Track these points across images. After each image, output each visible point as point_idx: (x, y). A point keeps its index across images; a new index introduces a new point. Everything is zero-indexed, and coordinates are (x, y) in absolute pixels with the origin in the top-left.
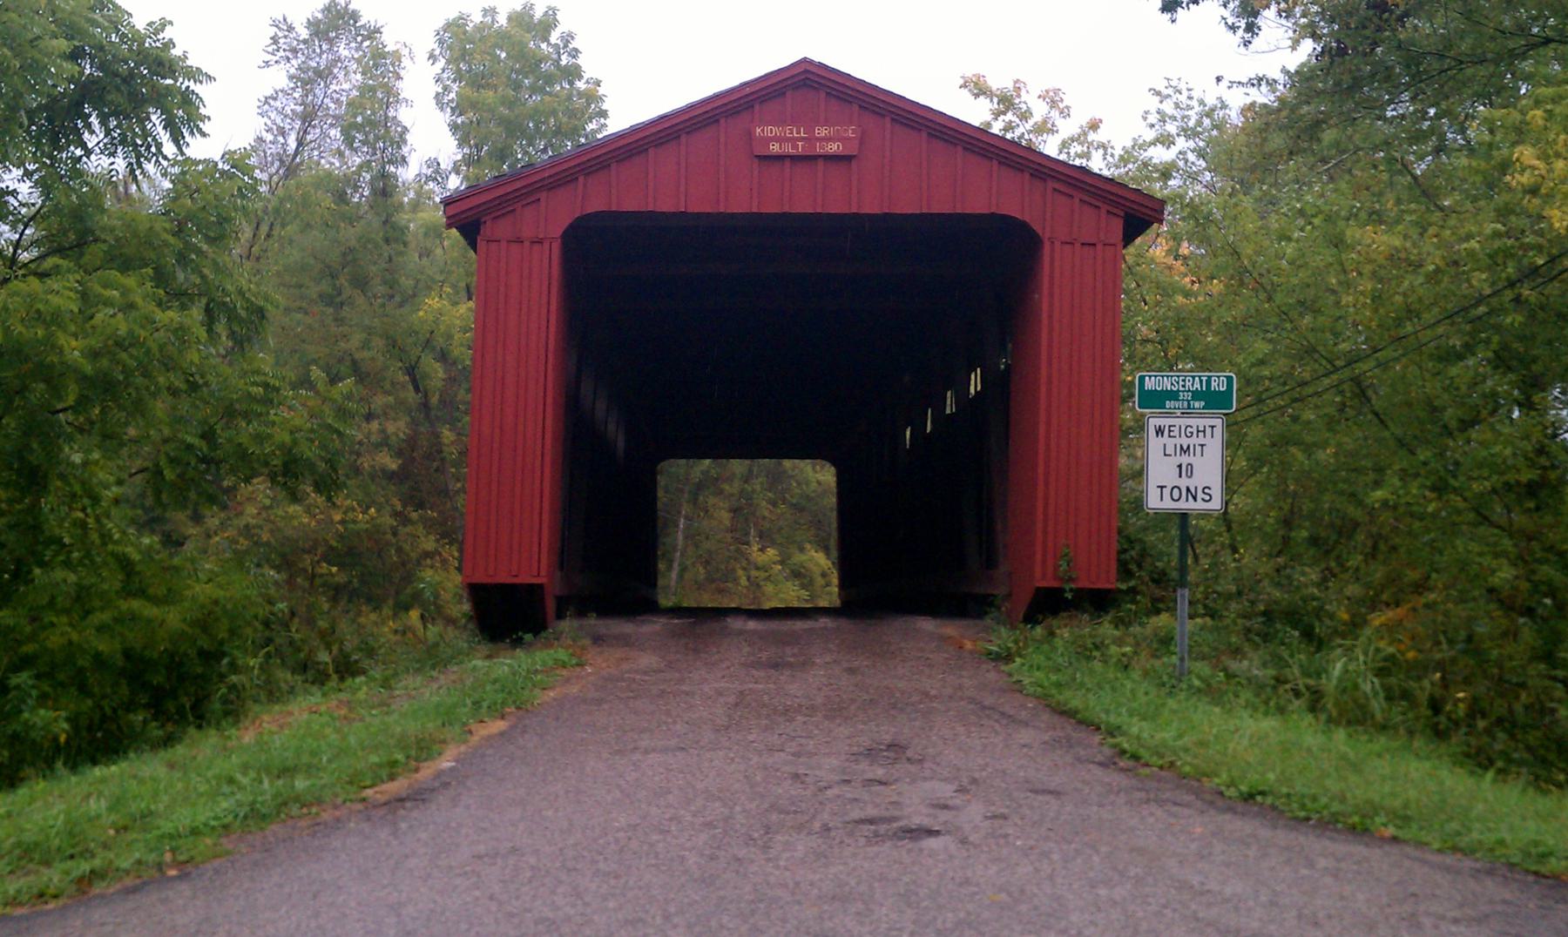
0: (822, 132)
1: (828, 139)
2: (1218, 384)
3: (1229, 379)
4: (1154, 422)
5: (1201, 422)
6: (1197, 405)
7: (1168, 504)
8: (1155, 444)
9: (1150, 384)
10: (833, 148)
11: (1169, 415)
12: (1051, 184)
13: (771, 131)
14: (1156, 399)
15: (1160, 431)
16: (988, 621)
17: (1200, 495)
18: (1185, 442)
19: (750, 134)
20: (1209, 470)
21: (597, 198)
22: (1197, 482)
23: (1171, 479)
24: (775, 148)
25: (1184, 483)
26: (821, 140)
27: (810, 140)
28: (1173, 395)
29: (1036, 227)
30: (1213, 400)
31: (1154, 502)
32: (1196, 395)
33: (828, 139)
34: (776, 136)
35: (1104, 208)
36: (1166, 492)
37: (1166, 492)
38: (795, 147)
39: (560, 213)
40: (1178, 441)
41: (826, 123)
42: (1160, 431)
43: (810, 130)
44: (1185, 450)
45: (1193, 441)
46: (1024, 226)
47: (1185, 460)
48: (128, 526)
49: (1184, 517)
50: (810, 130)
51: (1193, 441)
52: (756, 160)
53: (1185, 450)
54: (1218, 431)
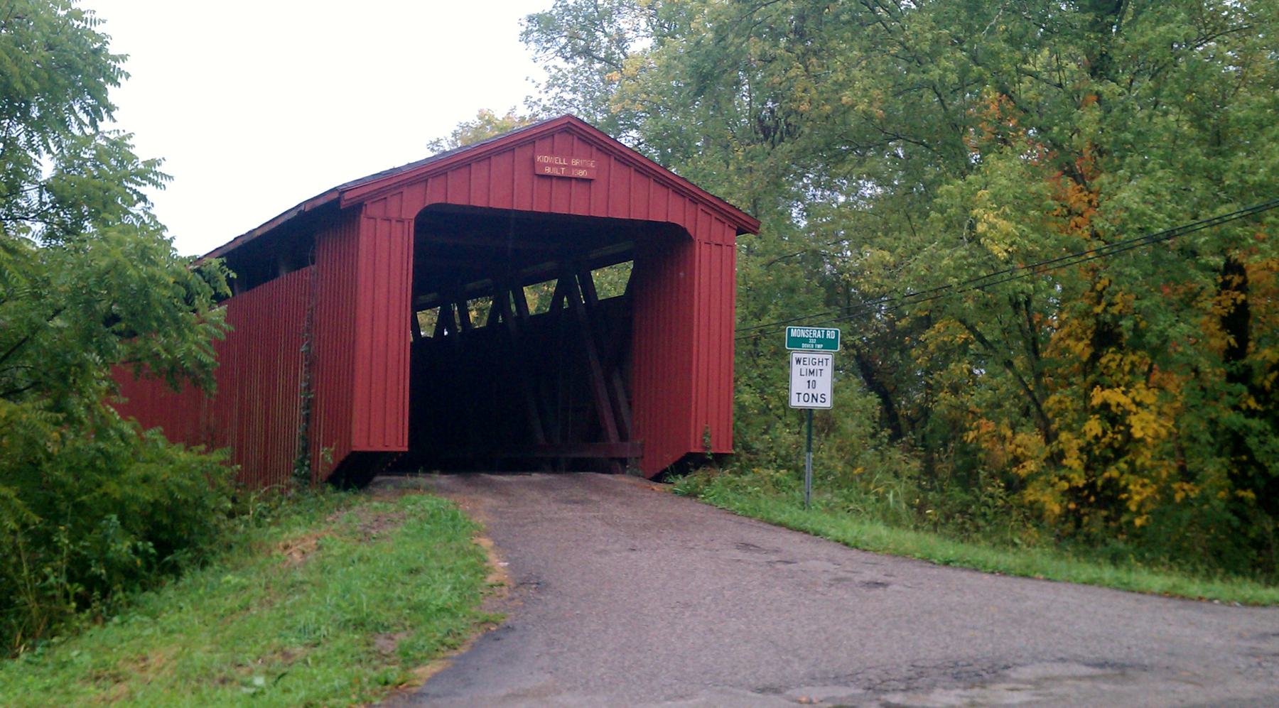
0: (575, 162)
1: (579, 167)
2: (831, 334)
3: (837, 332)
4: (795, 356)
5: (821, 357)
6: (819, 346)
7: (802, 404)
8: (795, 369)
9: (793, 333)
10: (582, 173)
11: (804, 352)
12: (700, 207)
13: (546, 159)
14: (798, 342)
15: (798, 361)
16: (370, 488)
17: (819, 399)
18: (812, 368)
19: (533, 160)
20: (824, 384)
21: (435, 196)
22: (817, 391)
23: (804, 389)
24: (548, 170)
25: (811, 391)
26: (575, 167)
27: (569, 167)
28: (806, 340)
29: (690, 230)
30: (827, 344)
31: (795, 402)
32: (819, 341)
33: (579, 167)
34: (550, 163)
35: (714, 215)
36: (801, 396)
37: (801, 396)
38: (560, 171)
39: (412, 205)
40: (808, 367)
41: (578, 157)
42: (798, 361)
43: (569, 161)
44: (812, 373)
45: (816, 367)
46: (684, 230)
47: (812, 378)
48: (1203, 491)
49: (810, 411)
50: (569, 161)
51: (816, 367)
52: (536, 178)
53: (812, 373)
54: (830, 362)
